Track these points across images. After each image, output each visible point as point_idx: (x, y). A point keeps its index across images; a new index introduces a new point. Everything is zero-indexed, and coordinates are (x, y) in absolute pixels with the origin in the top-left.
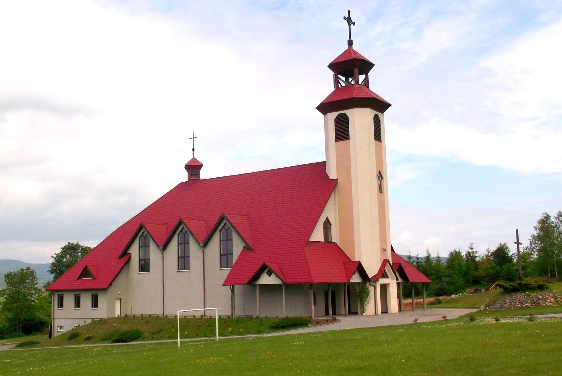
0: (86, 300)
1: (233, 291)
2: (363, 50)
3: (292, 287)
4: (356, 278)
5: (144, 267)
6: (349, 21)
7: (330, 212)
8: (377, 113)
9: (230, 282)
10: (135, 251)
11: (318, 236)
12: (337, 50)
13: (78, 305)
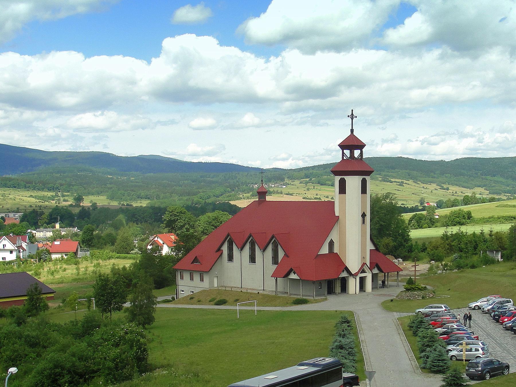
0: (197, 277)
1: (276, 280)
2: (361, 135)
3: (303, 281)
4: (344, 274)
5: (231, 258)
6: (352, 117)
7: (334, 236)
8: (364, 177)
9: (275, 275)
10: (225, 248)
11: (325, 250)
12: (344, 135)
13: (192, 279)
